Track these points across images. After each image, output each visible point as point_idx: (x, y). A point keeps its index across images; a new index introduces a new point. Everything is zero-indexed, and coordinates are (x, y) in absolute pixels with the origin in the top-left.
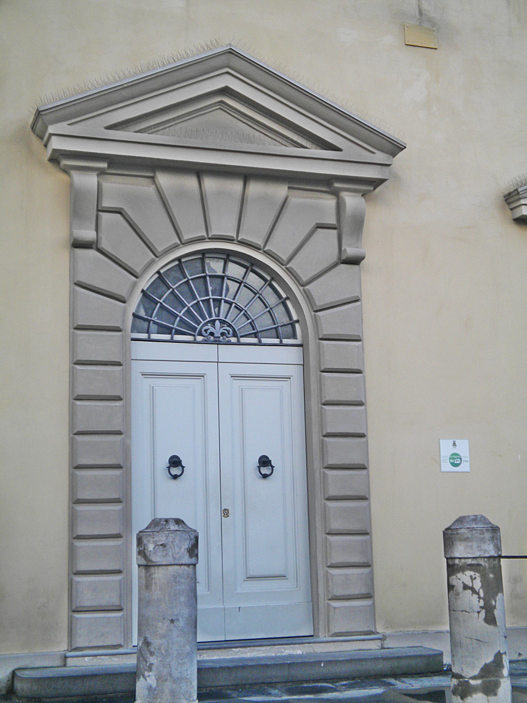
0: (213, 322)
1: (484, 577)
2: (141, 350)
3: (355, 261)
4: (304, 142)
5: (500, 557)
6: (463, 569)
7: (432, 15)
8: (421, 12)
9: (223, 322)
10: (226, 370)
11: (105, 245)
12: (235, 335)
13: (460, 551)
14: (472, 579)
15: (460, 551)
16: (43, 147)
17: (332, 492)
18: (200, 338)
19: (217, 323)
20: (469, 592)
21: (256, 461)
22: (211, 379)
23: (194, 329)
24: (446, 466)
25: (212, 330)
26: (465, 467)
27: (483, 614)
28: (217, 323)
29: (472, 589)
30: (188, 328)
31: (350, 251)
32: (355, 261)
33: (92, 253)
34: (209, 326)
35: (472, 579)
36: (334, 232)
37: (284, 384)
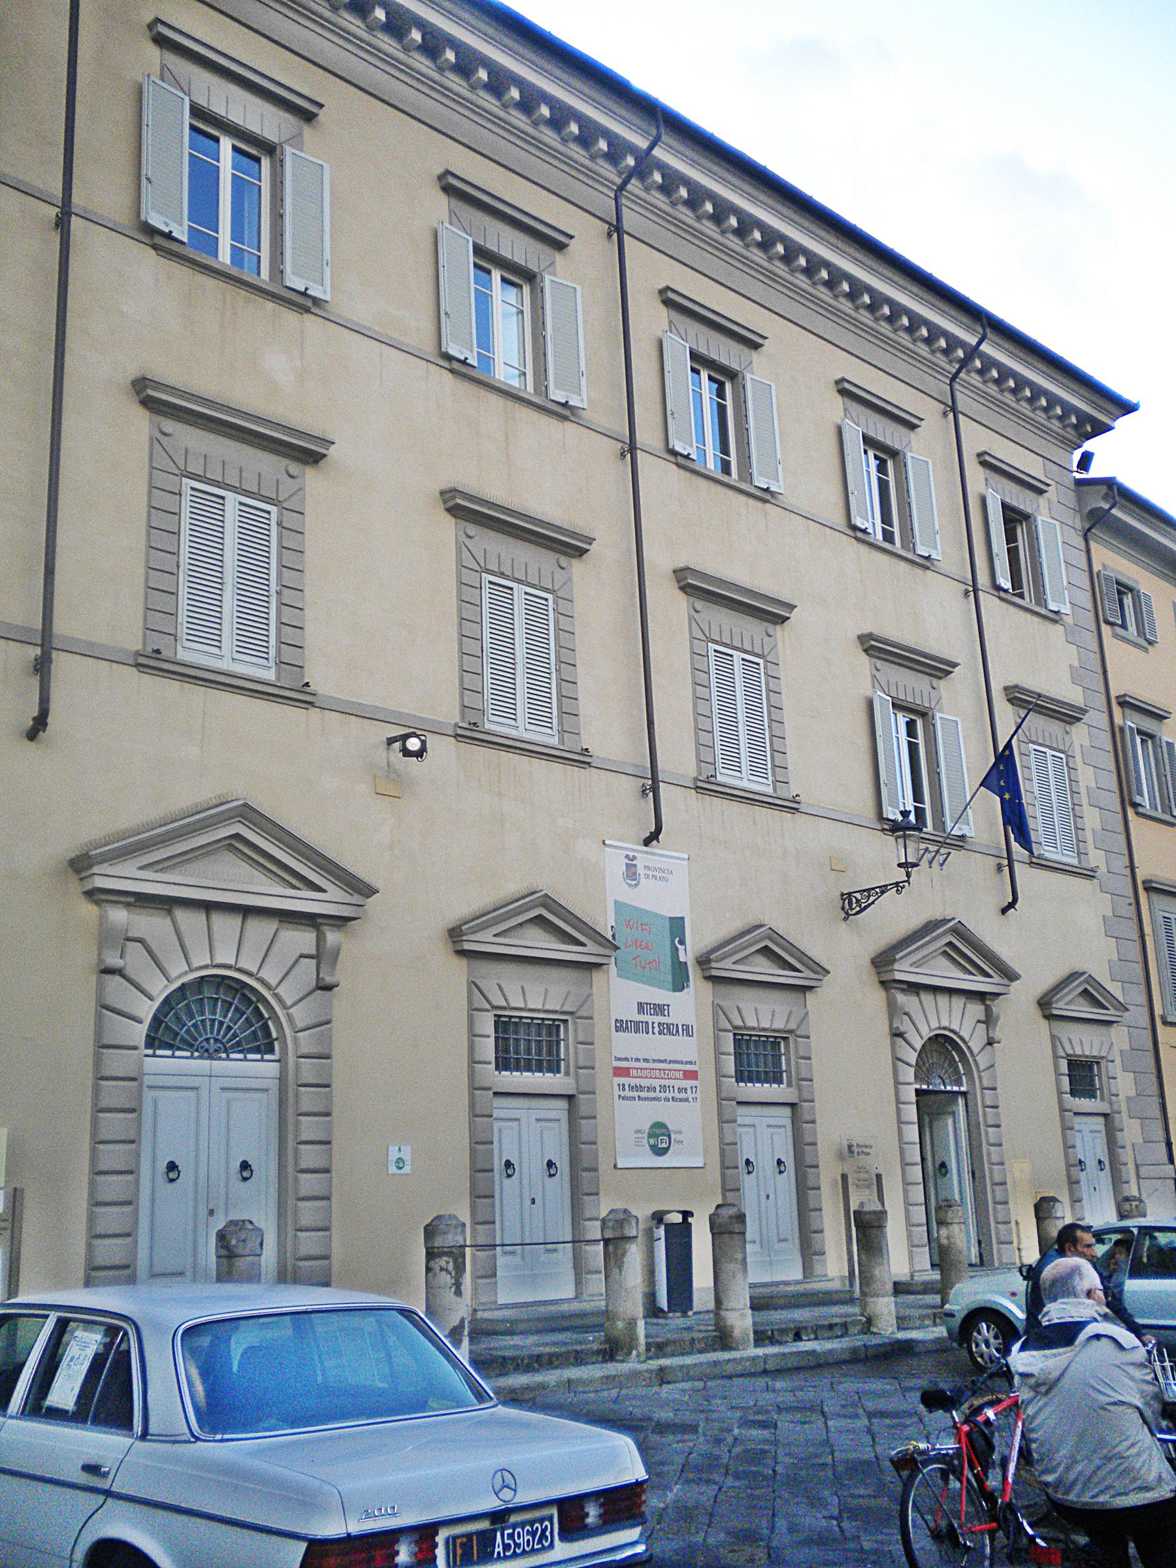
0: (207, 1040)
1: (455, 1261)
2: (151, 1064)
3: (328, 988)
4: (297, 884)
5: (573, 1242)
6: (440, 1255)
7: (397, 767)
8: (389, 765)
9: (216, 1040)
10: (218, 1083)
11: (129, 972)
12: (226, 1051)
13: (438, 1242)
14: (448, 1263)
15: (438, 1242)
16: (334, 1024)
17: (303, 1193)
18: (196, 1054)
19: (212, 1041)
20: (444, 1273)
21: (237, 1165)
22: (204, 1093)
23: (192, 1046)
24: (393, 1169)
25: (207, 1046)
26: (407, 1169)
27: (453, 1289)
28: (212, 1041)
29: (447, 1270)
30: (189, 1046)
31: (329, 980)
32: (328, 988)
33: (117, 978)
34: (204, 1043)
35: (448, 1263)
36: (314, 961)
37: (263, 1096)
